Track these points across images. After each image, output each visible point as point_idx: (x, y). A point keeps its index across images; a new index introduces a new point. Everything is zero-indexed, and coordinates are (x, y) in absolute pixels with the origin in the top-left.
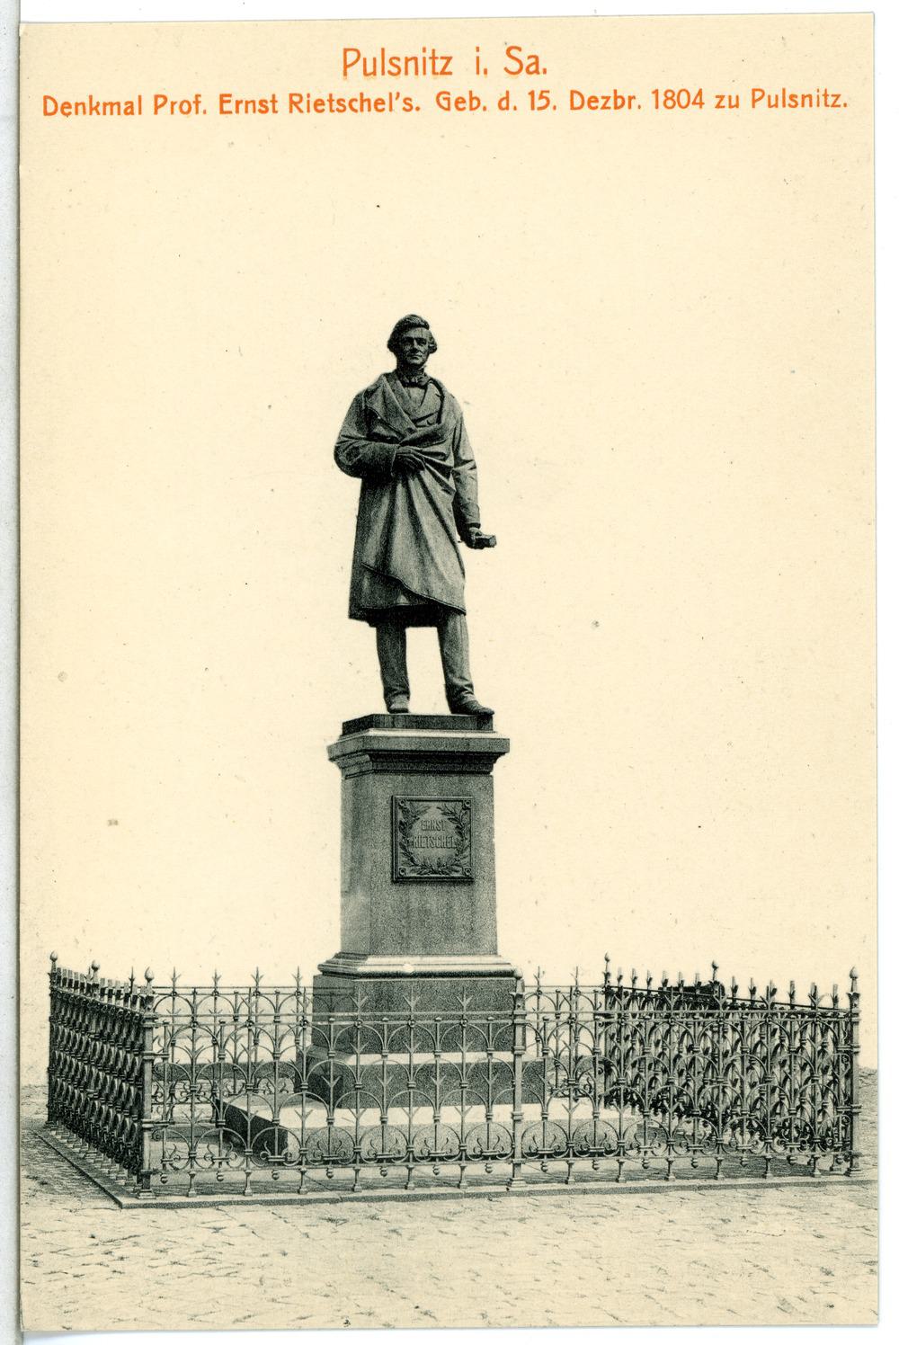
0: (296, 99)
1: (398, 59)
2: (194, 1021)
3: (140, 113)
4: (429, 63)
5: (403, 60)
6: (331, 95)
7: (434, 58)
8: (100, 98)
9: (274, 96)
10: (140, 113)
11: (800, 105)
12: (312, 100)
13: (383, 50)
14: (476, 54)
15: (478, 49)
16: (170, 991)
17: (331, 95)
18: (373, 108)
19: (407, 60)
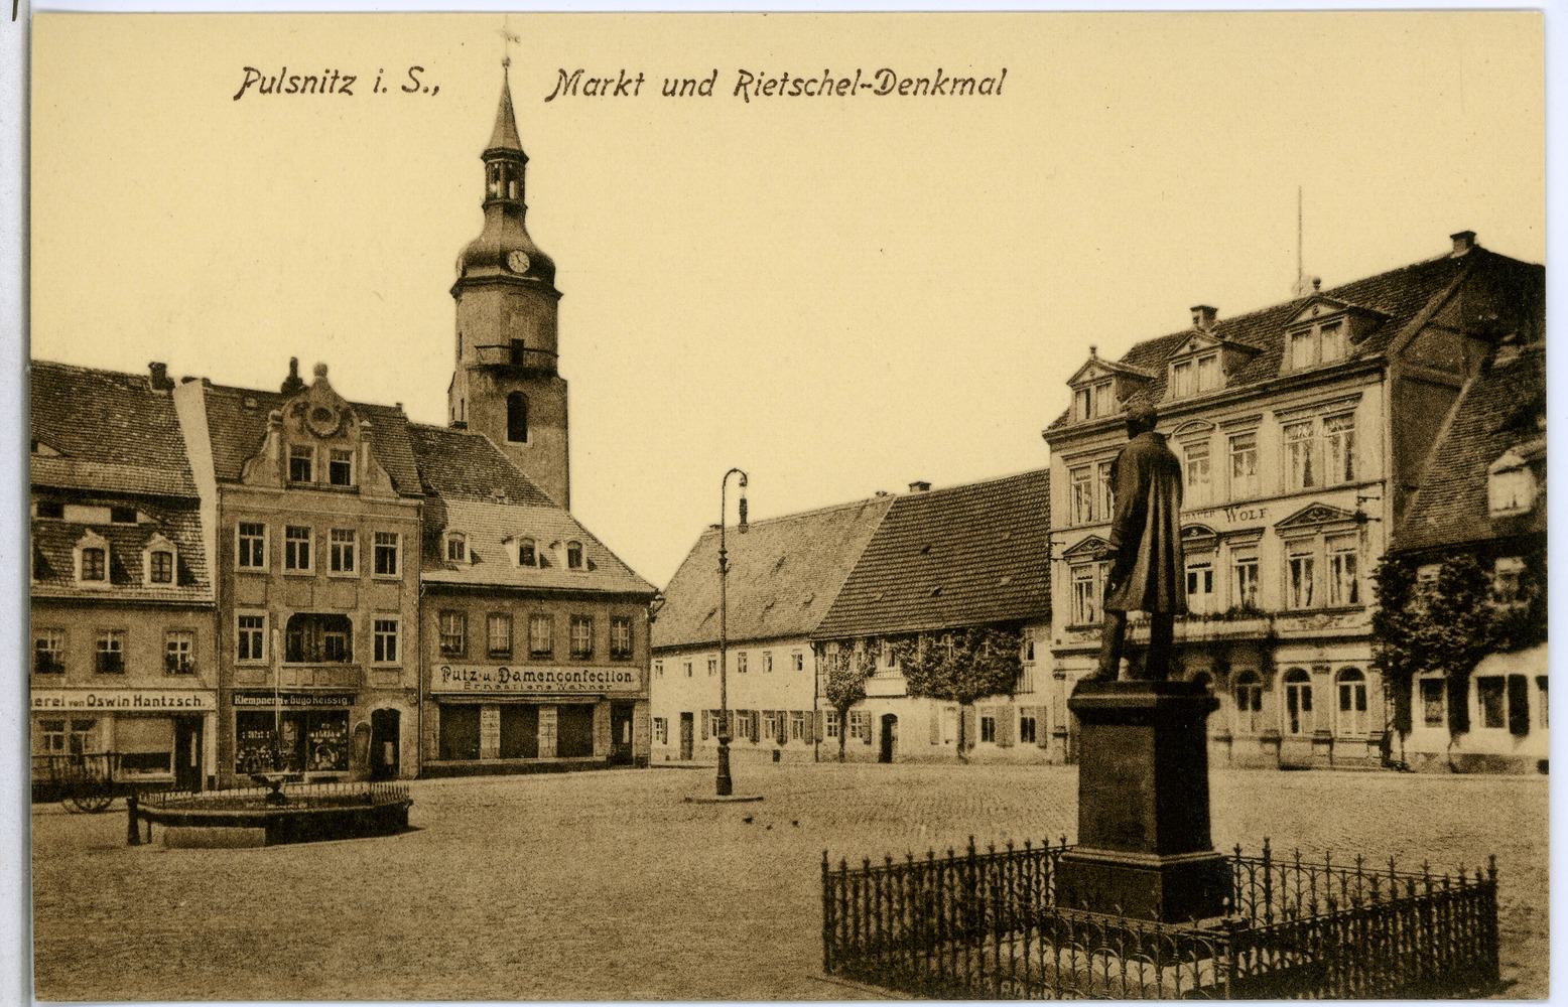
0: (747, 78)
1: (299, 78)
2: (1392, 872)
3: (1208, 589)
4: (329, 82)
5: (303, 80)
6: (786, 74)
7: (336, 77)
8: (828, 102)
9: (641, 75)
10: (1208, 589)
11: (791, 78)
12: (765, 80)
13: (285, 69)
14: (500, 49)
15: (381, 71)
16: (1355, 871)
17: (786, 74)
18: (761, 91)
19: (307, 79)
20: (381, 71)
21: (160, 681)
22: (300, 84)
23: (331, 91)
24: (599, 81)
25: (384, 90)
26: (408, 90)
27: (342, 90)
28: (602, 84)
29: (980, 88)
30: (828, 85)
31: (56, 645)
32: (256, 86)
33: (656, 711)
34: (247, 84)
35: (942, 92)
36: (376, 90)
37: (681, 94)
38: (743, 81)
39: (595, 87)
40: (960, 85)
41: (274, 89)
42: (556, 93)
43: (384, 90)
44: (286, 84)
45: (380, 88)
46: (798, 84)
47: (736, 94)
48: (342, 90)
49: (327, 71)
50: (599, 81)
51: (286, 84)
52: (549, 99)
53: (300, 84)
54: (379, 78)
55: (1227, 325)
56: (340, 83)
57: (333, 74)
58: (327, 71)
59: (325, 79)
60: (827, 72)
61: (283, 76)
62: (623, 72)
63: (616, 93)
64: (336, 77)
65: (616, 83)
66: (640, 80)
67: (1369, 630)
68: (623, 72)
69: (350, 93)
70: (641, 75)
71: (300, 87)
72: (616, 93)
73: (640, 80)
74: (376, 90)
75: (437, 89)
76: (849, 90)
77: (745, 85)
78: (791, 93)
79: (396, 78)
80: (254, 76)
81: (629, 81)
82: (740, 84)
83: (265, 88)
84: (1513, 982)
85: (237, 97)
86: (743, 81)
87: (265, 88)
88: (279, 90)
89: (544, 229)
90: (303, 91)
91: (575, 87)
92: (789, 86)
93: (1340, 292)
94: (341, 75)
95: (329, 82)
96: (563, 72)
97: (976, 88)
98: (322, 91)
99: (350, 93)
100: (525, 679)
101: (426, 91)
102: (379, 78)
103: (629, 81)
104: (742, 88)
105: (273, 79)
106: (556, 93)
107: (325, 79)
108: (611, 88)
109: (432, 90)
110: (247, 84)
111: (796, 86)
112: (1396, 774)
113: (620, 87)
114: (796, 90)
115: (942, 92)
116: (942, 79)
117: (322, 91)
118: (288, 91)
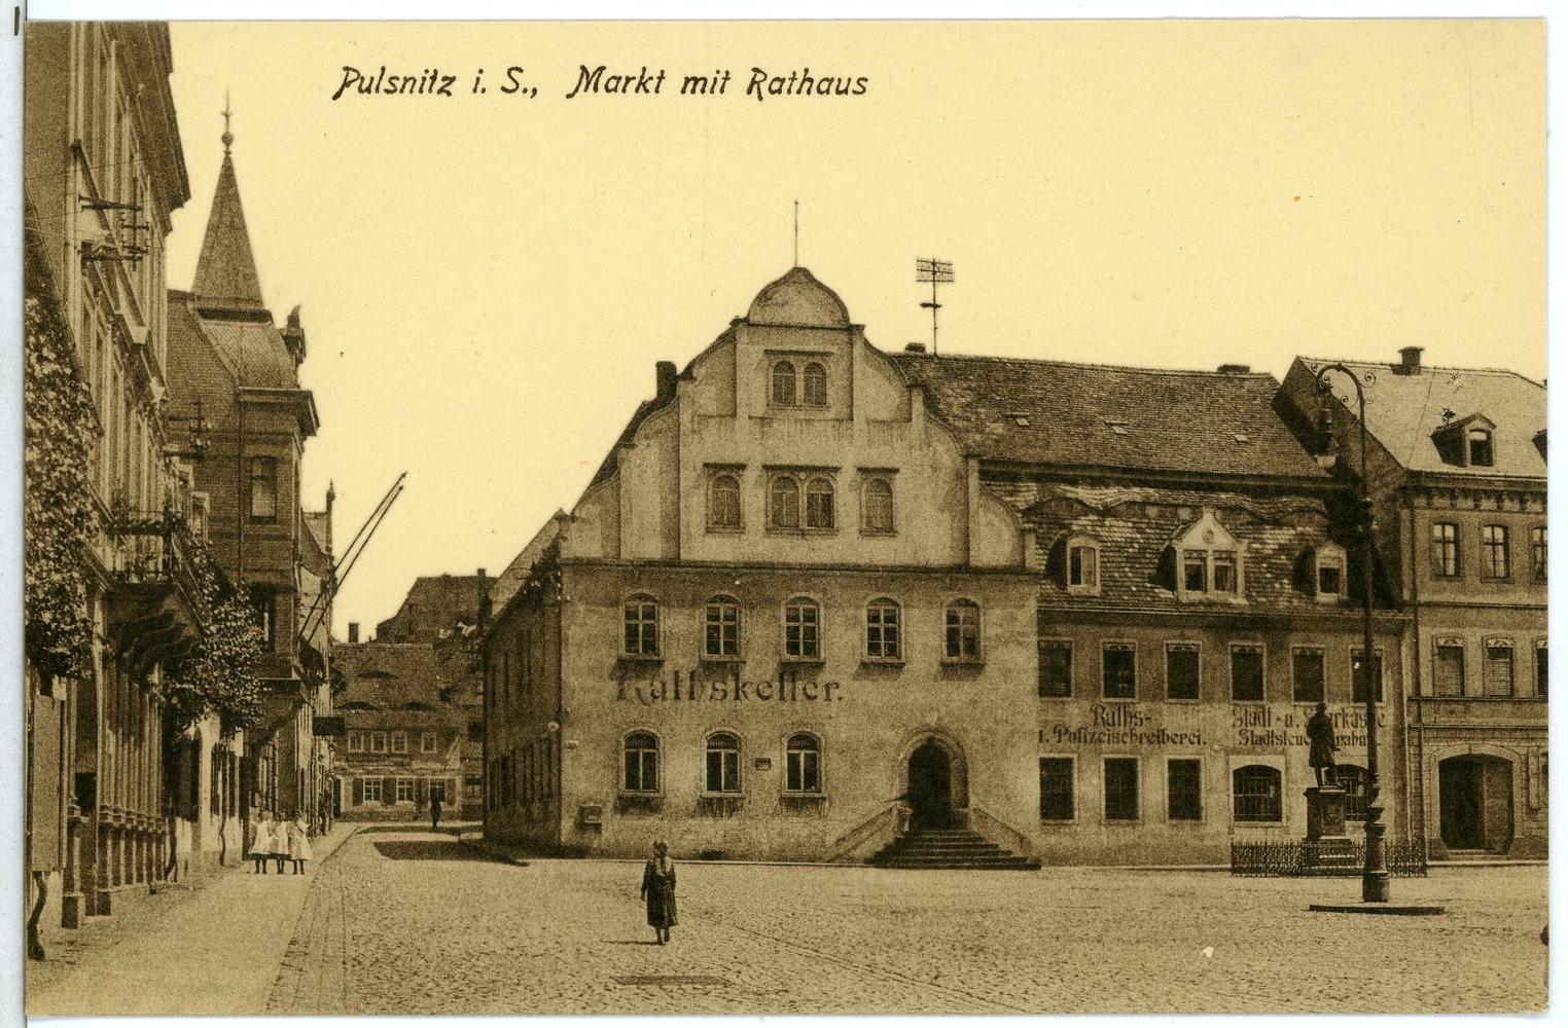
0: (760, 77)
9: (662, 72)
15: (481, 71)
17: (794, 73)
20: (481, 71)
21: (73, 772)
22: (399, 84)
23: (430, 90)
24: (833, 79)
26: (858, 93)
27: (441, 91)
28: (623, 81)
29: (819, 87)
30: (807, 84)
31: (1448, 670)
34: (346, 84)
35: (647, 91)
36: (475, 90)
37: (799, 92)
38: (757, 79)
39: (618, 84)
40: (691, 83)
42: (577, 90)
43: (483, 91)
44: (385, 84)
46: (394, 81)
47: (749, 91)
48: (441, 91)
49: (718, 72)
50: (833, 79)
51: (385, 84)
52: (569, 96)
54: (478, 79)
56: (439, 84)
57: (431, 73)
58: (718, 72)
59: (715, 79)
60: (806, 70)
61: (381, 79)
62: (644, 69)
63: (637, 90)
65: (638, 80)
66: (661, 78)
68: (644, 69)
69: (449, 94)
70: (662, 72)
71: (399, 86)
72: (637, 90)
73: (661, 78)
74: (475, 90)
77: (758, 83)
78: (387, 91)
79: (496, 78)
80: (353, 75)
82: (753, 82)
83: (841, 89)
84: (47, 690)
85: (337, 96)
86: (757, 79)
87: (841, 89)
90: (402, 91)
91: (597, 80)
92: (439, 84)
96: (583, 68)
98: (421, 91)
99: (449, 94)
100: (1189, 596)
102: (478, 79)
103: (651, 78)
104: (756, 86)
105: (372, 79)
106: (577, 90)
107: (715, 79)
108: (633, 84)
110: (346, 84)
111: (393, 85)
113: (642, 84)
115: (647, 91)
117: (421, 91)
118: (387, 91)
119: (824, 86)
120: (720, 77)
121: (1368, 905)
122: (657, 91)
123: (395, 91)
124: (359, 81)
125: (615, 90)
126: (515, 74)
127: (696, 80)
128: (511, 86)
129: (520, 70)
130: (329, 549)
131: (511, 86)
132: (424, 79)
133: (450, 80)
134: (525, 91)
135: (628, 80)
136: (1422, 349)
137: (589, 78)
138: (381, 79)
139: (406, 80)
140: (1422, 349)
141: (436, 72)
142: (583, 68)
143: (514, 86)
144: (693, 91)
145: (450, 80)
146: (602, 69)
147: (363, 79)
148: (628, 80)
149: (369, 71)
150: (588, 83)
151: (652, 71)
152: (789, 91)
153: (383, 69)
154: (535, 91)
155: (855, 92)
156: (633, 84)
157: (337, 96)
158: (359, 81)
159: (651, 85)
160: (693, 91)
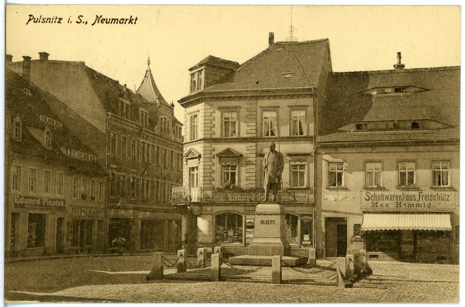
7: (56, 18)
11: (58, 18)
15: (70, 17)
22: (46, 20)
25: (71, 22)
26: (43, 23)
32: (33, 20)
33: (245, 153)
34: (30, 20)
36: (68, 22)
40: (114, 21)
41: (38, 22)
43: (71, 22)
44: (41, 20)
45: (70, 22)
50: (124, 19)
51: (41, 20)
53: (46, 20)
54: (69, 19)
55: (408, 72)
56: (58, 20)
61: (40, 18)
63: (129, 23)
64: (56, 18)
65: (129, 20)
66: (136, 19)
67: (270, 278)
68: (131, 17)
70: (137, 18)
71: (46, 21)
72: (129, 23)
73: (136, 19)
74: (68, 22)
75: (87, 23)
76: (105, 22)
79: (75, 19)
80: (32, 18)
81: (133, 19)
88: (39, 22)
89: (150, 59)
90: (46, 22)
93: (415, 71)
94: (58, 18)
95: (54, 20)
96: (97, 16)
97: (118, 22)
101: (84, 22)
102: (69, 19)
105: (38, 19)
108: (128, 21)
109: (85, 23)
110: (30, 20)
112: (390, 211)
114: (43, 21)
116: (132, 19)
119: (122, 21)
120: (54, 18)
121: (212, 89)
122: (135, 23)
123: (45, 22)
124: (34, 19)
125: (123, 23)
126: (80, 18)
127: (115, 20)
128: (79, 21)
129: (82, 16)
130: (160, 98)
131: (79, 21)
132: (53, 19)
133: (61, 19)
134: (84, 22)
135: (127, 20)
136: (49, 55)
137: (100, 19)
138: (40, 18)
139: (48, 19)
140: (49, 55)
141: (57, 17)
142: (97, 16)
143: (80, 21)
144: (114, 23)
145: (61, 19)
146: (101, 16)
147: (35, 19)
148: (127, 20)
149: (36, 16)
150: (99, 21)
151: (134, 17)
152: (55, 22)
153: (41, 16)
154: (87, 23)
155: (42, 22)
156: (128, 21)
157: (27, 23)
158: (34, 19)
159: (133, 21)
160: (114, 23)
